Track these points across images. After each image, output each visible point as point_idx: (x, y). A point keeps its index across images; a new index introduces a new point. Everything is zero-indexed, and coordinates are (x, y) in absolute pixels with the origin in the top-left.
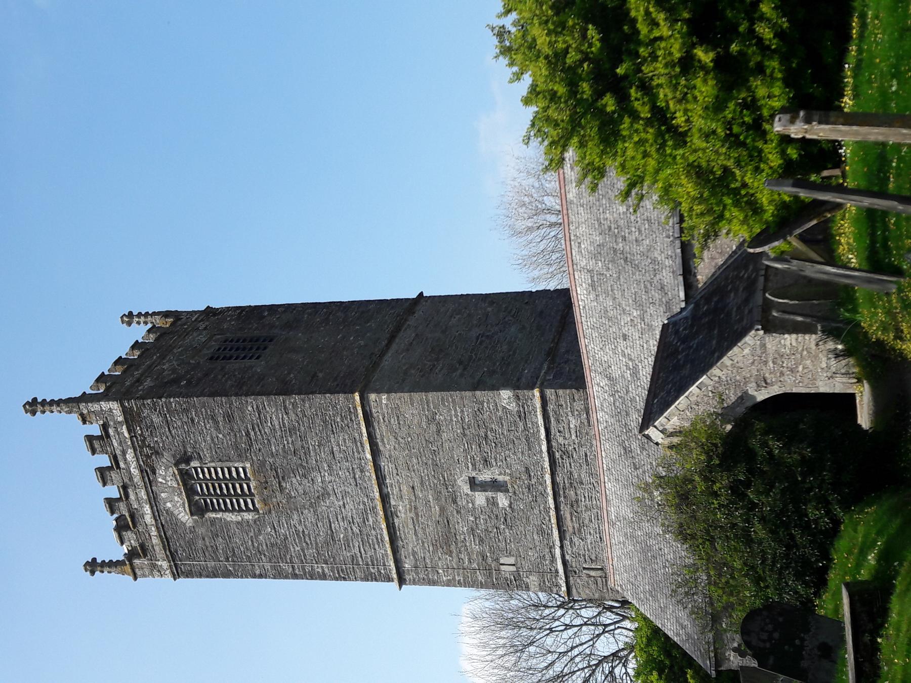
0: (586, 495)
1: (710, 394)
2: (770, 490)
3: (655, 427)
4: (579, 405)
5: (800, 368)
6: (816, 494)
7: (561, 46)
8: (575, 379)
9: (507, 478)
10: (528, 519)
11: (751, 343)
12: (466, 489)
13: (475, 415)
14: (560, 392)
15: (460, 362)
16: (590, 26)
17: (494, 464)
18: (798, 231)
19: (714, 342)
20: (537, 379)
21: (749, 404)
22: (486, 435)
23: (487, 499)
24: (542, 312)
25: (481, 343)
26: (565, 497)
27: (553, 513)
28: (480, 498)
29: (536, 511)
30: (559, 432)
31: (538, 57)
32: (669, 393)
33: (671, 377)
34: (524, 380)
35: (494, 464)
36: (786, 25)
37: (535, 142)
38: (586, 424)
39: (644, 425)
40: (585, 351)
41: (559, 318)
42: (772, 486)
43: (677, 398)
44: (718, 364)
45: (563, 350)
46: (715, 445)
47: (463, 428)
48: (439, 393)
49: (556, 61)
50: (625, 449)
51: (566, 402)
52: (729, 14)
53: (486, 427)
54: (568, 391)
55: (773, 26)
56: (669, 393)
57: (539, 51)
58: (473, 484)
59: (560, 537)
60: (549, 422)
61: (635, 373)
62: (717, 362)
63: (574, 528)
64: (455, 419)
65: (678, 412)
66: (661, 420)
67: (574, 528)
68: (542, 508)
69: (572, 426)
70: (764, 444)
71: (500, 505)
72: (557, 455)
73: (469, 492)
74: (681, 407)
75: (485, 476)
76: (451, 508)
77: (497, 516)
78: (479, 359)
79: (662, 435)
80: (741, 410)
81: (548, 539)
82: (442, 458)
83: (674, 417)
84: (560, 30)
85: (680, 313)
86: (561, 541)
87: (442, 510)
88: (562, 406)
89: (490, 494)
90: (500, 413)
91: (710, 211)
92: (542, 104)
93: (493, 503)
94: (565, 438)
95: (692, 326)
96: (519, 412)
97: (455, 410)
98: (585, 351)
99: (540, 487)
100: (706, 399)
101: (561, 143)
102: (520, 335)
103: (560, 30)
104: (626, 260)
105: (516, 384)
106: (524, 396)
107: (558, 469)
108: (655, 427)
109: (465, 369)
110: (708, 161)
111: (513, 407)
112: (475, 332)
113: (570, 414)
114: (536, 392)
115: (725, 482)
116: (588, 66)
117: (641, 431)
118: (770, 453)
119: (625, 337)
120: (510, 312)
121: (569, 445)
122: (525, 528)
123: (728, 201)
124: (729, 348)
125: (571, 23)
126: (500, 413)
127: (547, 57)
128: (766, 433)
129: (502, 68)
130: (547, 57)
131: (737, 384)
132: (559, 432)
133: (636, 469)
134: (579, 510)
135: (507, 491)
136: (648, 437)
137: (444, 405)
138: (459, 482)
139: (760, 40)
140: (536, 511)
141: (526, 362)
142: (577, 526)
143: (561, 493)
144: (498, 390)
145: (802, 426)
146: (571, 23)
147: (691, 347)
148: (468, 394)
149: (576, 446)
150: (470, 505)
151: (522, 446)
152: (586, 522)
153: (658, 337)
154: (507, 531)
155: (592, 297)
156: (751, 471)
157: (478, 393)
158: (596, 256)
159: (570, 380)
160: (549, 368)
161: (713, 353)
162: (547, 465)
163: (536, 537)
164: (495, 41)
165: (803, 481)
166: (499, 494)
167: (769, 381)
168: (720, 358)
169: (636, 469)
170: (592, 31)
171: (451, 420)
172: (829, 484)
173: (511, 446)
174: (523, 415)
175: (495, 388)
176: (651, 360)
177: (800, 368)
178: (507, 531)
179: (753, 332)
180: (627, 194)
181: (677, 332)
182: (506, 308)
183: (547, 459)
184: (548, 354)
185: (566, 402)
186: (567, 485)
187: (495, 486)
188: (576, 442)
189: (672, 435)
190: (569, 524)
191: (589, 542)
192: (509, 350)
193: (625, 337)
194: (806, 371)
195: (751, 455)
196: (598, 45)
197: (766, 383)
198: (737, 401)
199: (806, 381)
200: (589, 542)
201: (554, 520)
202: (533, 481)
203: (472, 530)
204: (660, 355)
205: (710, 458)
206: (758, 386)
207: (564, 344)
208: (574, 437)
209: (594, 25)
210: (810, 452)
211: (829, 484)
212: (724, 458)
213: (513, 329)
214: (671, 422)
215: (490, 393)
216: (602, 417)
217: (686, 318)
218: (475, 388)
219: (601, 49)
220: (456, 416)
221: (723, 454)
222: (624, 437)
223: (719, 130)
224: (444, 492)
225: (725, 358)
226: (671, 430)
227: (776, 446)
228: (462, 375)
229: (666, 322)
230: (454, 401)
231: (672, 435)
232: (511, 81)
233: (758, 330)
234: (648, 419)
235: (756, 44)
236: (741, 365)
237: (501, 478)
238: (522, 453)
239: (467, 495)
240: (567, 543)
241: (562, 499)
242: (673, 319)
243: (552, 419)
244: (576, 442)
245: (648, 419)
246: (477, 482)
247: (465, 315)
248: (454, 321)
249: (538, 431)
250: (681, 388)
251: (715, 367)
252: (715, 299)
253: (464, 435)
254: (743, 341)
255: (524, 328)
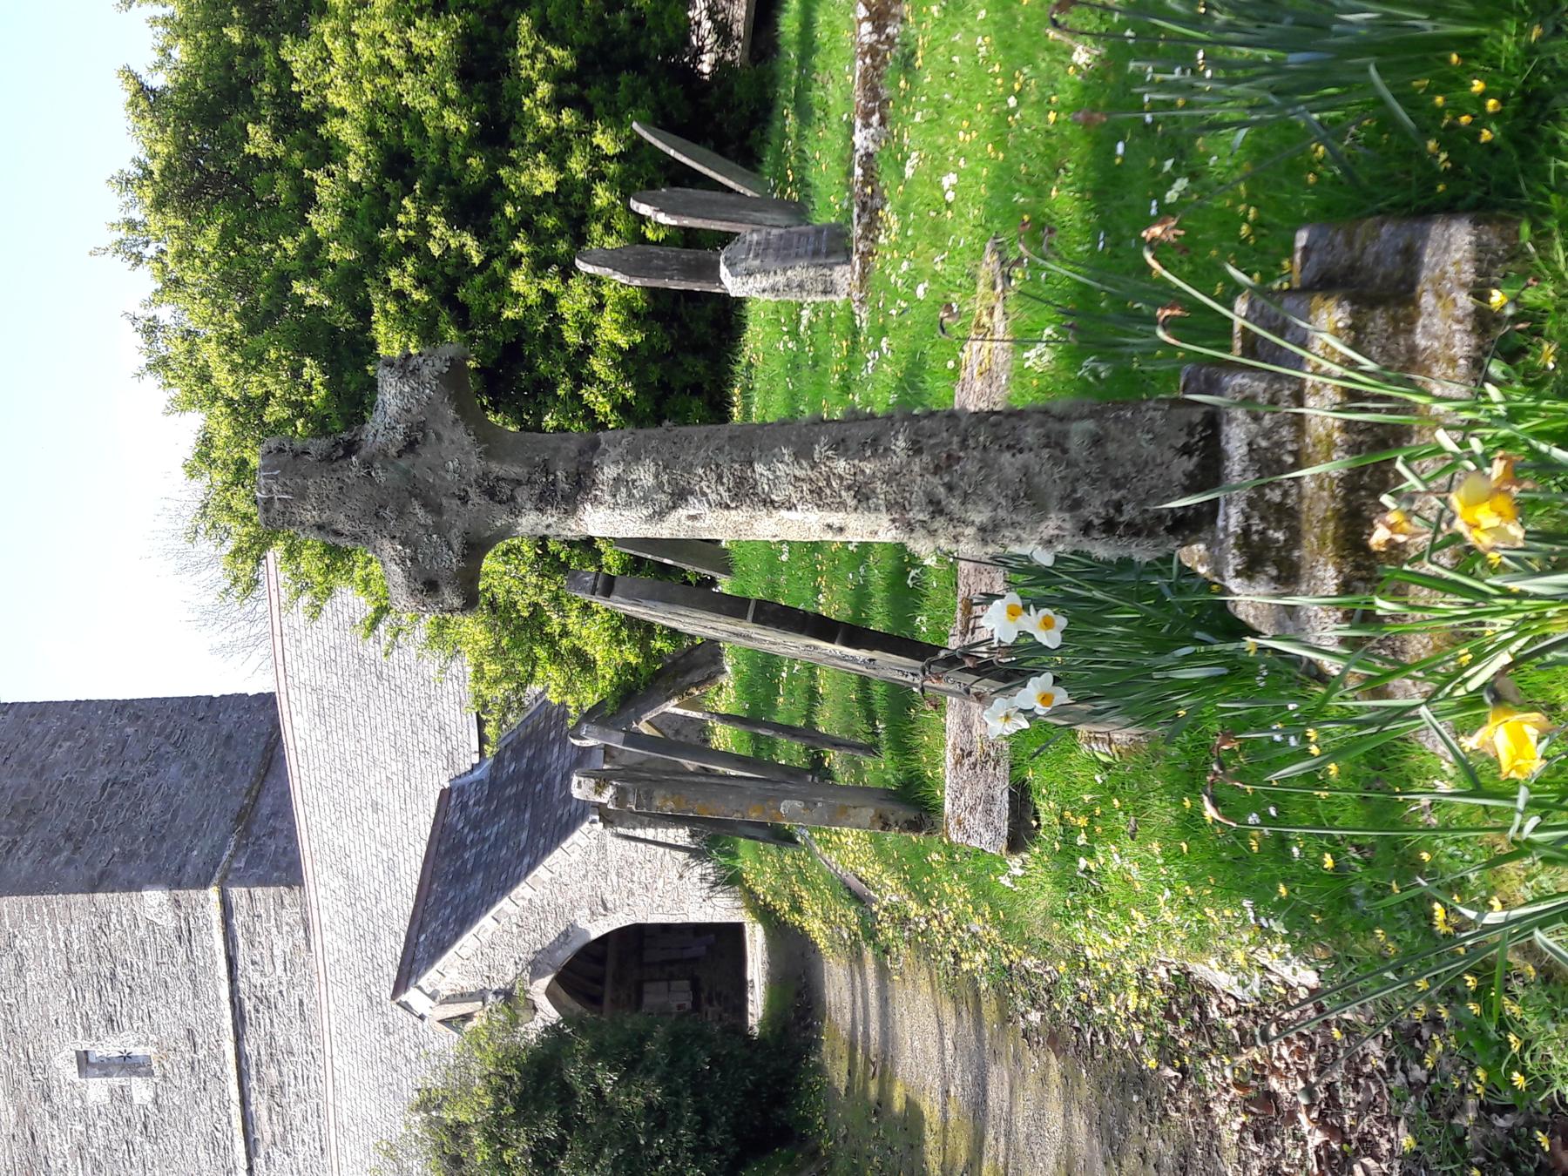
0: (299, 1075)
1: (515, 929)
2: (595, 1161)
3: (420, 988)
4: (290, 915)
5: (660, 884)
6: (667, 1167)
7: (255, 391)
8: (284, 869)
9: (151, 1050)
10: (188, 1123)
11: (583, 843)
12: (71, 1072)
13: (93, 938)
14: (258, 892)
15: (68, 836)
16: (308, 361)
17: (127, 1025)
18: (650, 715)
19: (524, 836)
20: (215, 867)
21: (577, 944)
22: (113, 974)
23: (111, 1091)
24: (229, 737)
25: (111, 797)
26: (259, 1080)
27: (235, 1110)
28: (97, 1089)
29: (205, 1107)
30: (254, 963)
31: (214, 400)
32: (445, 924)
33: (451, 894)
34: (189, 868)
35: (127, 1025)
36: (630, 393)
37: (205, 547)
38: (303, 947)
39: (401, 985)
40: (303, 827)
41: (261, 748)
42: (598, 1152)
43: (457, 936)
44: (529, 879)
45: (266, 811)
46: (509, 1079)
47: (69, 962)
48: (23, 899)
49: (247, 410)
50: (370, 998)
51: (267, 911)
52: (543, 366)
53: (114, 959)
54: (272, 890)
55: (610, 394)
56: (445, 924)
57: (217, 390)
58: (84, 1062)
59: (248, 1153)
60: (235, 946)
61: (391, 868)
62: (526, 875)
63: (274, 1135)
64: (51, 946)
65: (460, 961)
66: (429, 979)
67: (274, 1135)
68: (215, 1102)
69: (276, 952)
70: (591, 1076)
71: (137, 1101)
72: (248, 1006)
73: (76, 1078)
74: (465, 953)
75: (109, 1048)
76: (40, 1110)
77: (128, 1120)
78: (106, 830)
79: (430, 1002)
80: (564, 955)
81: (225, 1158)
82: (24, 1019)
83: (455, 969)
84: (253, 363)
85: (472, 771)
86: (249, 1159)
87: (22, 1114)
88: (259, 916)
89: (116, 1081)
90: (140, 934)
91: (508, 675)
92: (218, 477)
93: (123, 1096)
94: (263, 973)
95: (489, 798)
96: (179, 929)
97: (55, 929)
98: (303, 827)
99: (214, 1065)
100: (507, 938)
101: (253, 550)
102: (186, 782)
103: (253, 363)
104: (380, 677)
105: (176, 880)
106: (189, 899)
107: (248, 1029)
108: (420, 988)
109: (77, 848)
110: (509, 592)
111: (168, 921)
112: (100, 776)
113: (274, 930)
114: (213, 893)
115: (524, 1146)
116: (304, 426)
117: (395, 995)
118: (598, 1092)
119: (376, 807)
120: (168, 737)
121: (271, 986)
122: (182, 1138)
123: (540, 652)
124: (548, 850)
125: (273, 355)
126: (140, 934)
127: (230, 402)
128: (592, 1058)
129: (154, 393)
130: (230, 402)
131: (558, 911)
132: (254, 963)
133: (388, 1033)
134: (284, 1101)
135: (150, 1073)
136: (406, 1007)
137: (32, 920)
138: (58, 1062)
139: (590, 413)
140: (205, 1107)
141: (196, 833)
142: (278, 1130)
143: (253, 1072)
144: (139, 890)
145: (649, 1046)
146: (273, 355)
147: (485, 840)
148: (81, 898)
149: (284, 989)
150: (78, 1103)
151: (183, 990)
152: (297, 1122)
153: (433, 810)
154: (147, 1146)
155: (319, 733)
156: (565, 1123)
157: (100, 896)
158: (328, 664)
159: (277, 868)
160: (237, 847)
161: (521, 856)
162: (227, 1023)
163: (202, 1155)
164: (139, 340)
165: (648, 1145)
166: (134, 1079)
167: (609, 905)
168: (531, 867)
169: (388, 1033)
170: (311, 370)
171: (46, 947)
172: (688, 1150)
173: (160, 992)
174: (184, 936)
175: (132, 886)
176: (422, 848)
177: (660, 884)
178: (147, 1146)
179: (586, 825)
180: (374, 625)
181: (464, 807)
182: (163, 728)
183: (228, 1013)
184: (239, 819)
185: (267, 911)
186: (264, 1058)
187: (128, 1065)
188: (284, 980)
189: (448, 1000)
190: (265, 1129)
191: (301, 1157)
192: (163, 813)
193: (376, 807)
194: (668, 887)
195: (567, 1094)
196: (323, 392)
197: (606, 909)
198: (558, 939)
199: (668, 903)
200: (301, 1157)
201: (237, 1123)
202: (201, 1053)
203: (80, 1148)
204: (434, 849)
205: (500, 1104)
206: (593, 913)
207: (269, 800)
208: (280, 971)
209: (313, 357)
210: (661, 1095)
211: (688, 1150)
212: (522, 1102)
213: (173, 769)
214: (447, 979)
215: (124, 897)
216: (332, 940)
217: (480, 782)
218: (93, 889)
219: (326, 399)
220: (56, 939)
221: (522, 1095)
222: (369, 977)
223: (525, 548)
224: (27, 1080)
225: (540, 868)
226: (448, 993)
227: (607, 1080)
228: (69, 862)
229: (447, 785)
230: (51, 913)
231: (448, 1000)
232: (168, 412)
233: (593, 822)
234: (408, 972)
235: (585, 418)
236: (565, 879)
237: (138, 1051)
238: (182, 1003)
239: (73, 1084)
240: (259, 1162)
241: (254, 1083)
242: (459, 781)
243: (241, 941)
244: (284, 980)
245: (408, 972)
246: (92, 1059)
247: (82, 741)
248: (58, 753)
249: (214, 963)
250: (465, 920)
251: (523, 884)
252: (529, 753)
253: (70, 974)
254: (569, 841)
255: (195, 767)
